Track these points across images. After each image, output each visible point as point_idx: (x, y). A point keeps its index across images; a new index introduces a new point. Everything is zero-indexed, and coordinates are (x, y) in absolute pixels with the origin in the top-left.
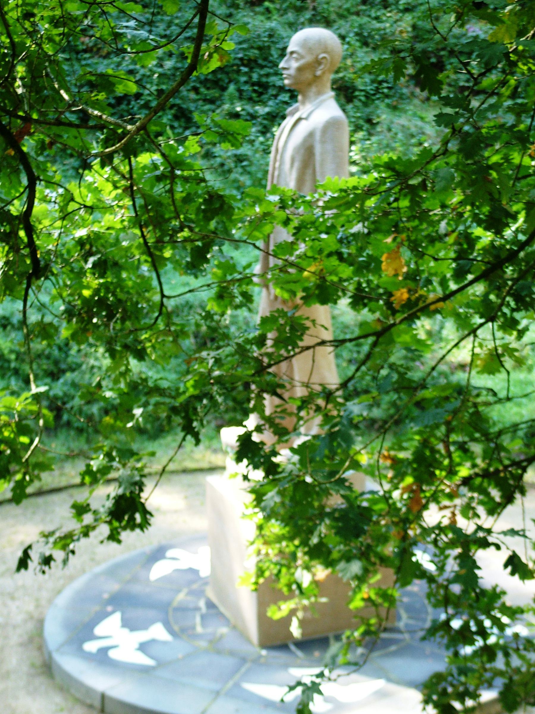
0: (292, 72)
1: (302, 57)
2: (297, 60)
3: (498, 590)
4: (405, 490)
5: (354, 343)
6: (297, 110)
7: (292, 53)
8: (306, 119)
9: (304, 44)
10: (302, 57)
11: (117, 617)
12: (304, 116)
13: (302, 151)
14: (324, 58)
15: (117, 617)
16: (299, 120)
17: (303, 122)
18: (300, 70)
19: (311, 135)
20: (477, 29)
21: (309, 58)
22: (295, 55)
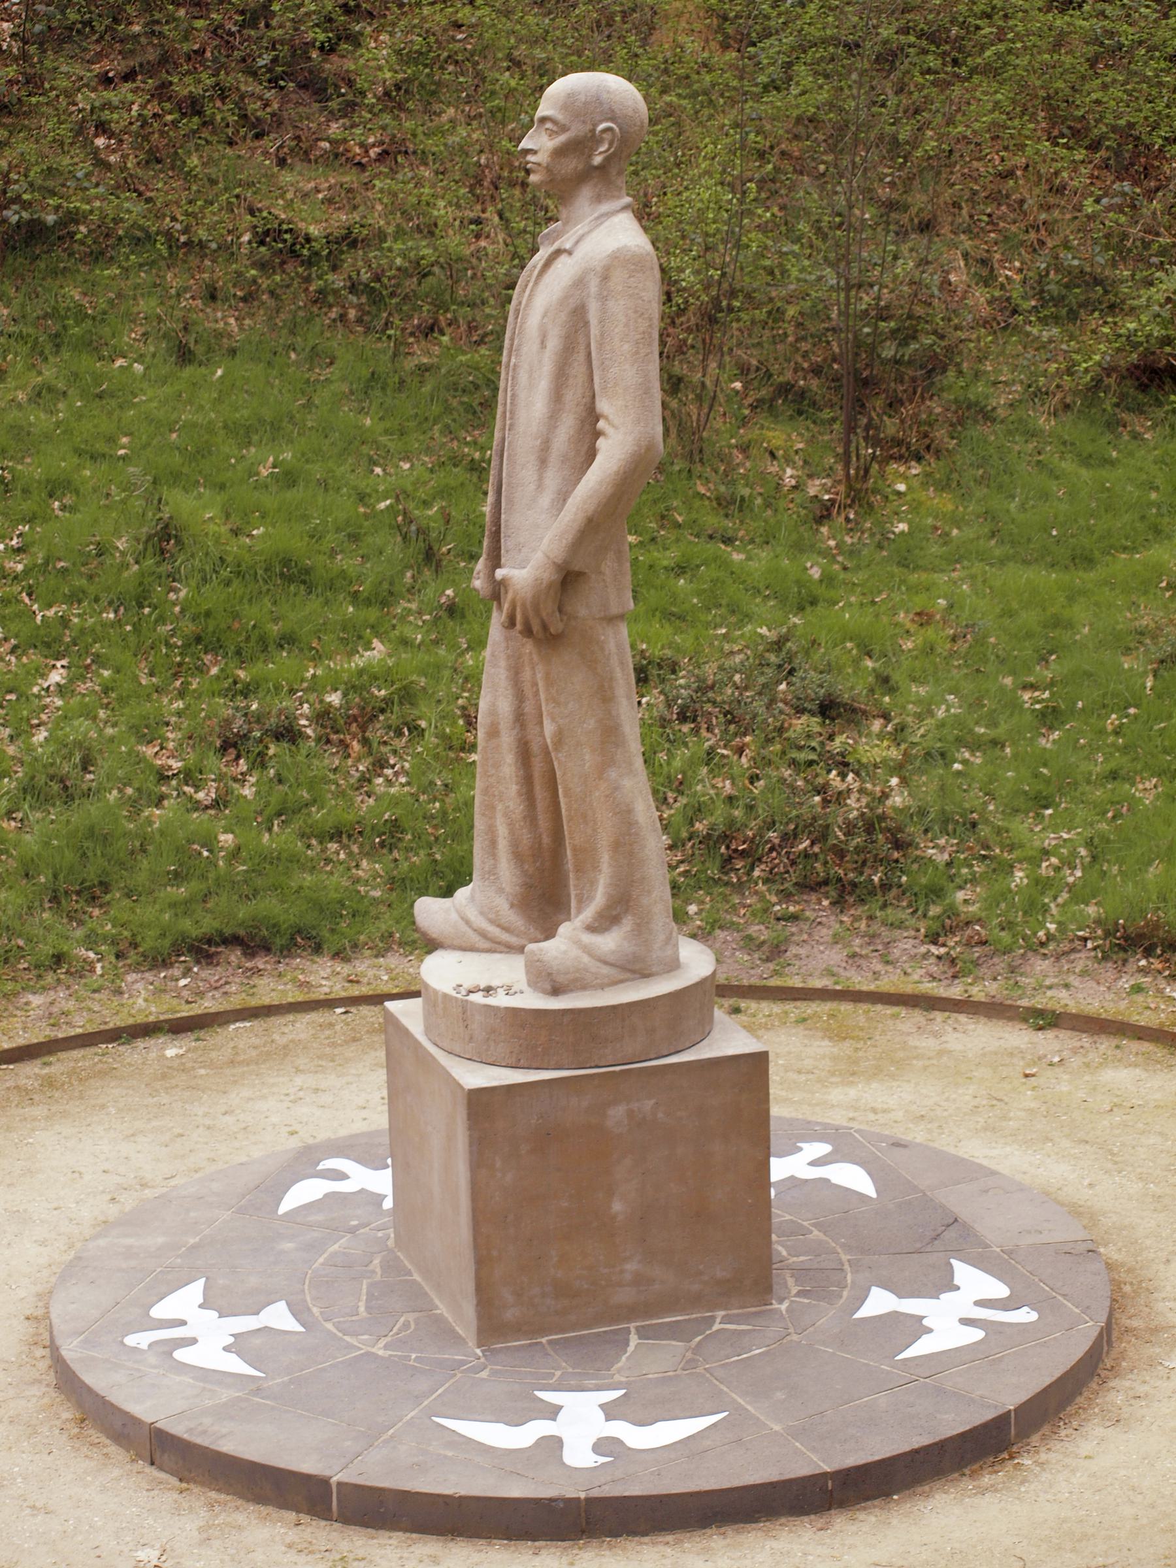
0: (541, 158)
1: (563, 129)
2: (552, 134)
3: (925, 1322)
4: (973, 755)
5: (314, 996)
6: (558, 235)
7: (543, 120)
8: (569, 253)
9: (569, 103)
10: (563, 129)
11: (195, 1290)
12: (568, 246)
13: (563, 316)
14: (609, 129)
15: (195, 1290)
16: (558, 252)
17: (563, 258)
18: (560, 153)
19: (580, 283)
20: (135, 107)
21: (577, 130)
22: (549, 125)
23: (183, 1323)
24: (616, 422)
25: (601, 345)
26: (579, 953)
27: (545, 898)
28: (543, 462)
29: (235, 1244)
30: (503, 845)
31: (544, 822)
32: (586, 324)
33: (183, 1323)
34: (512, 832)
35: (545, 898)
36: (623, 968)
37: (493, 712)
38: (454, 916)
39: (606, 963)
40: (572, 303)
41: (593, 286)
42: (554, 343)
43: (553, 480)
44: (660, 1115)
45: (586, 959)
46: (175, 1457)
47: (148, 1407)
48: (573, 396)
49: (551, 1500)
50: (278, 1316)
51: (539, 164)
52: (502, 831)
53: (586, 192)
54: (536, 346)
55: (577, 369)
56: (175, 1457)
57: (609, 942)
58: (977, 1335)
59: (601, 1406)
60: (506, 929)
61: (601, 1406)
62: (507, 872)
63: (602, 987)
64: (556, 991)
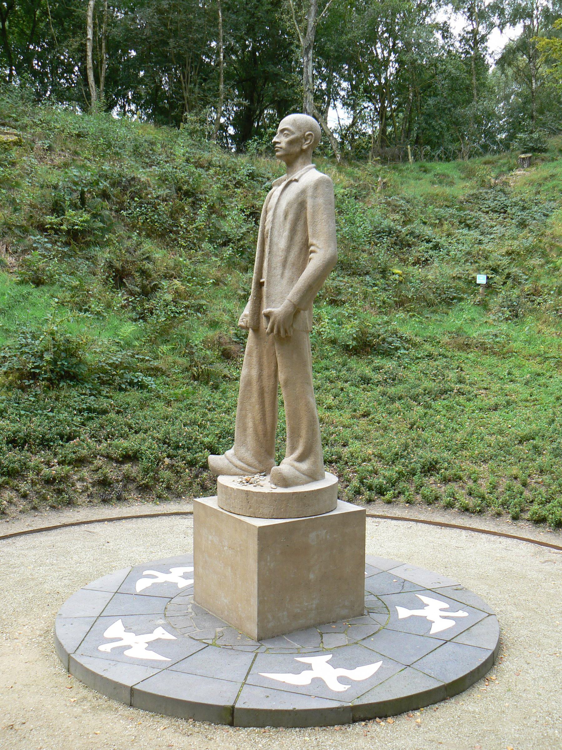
8: (296, 181)
10: (293, 133)
12: (296, 178)
21: (297, 134)
22: (285, 132)
23: (121, 639)
24: (320, 247)
25: (313, 217)
26: (294, 470)
27: (268, 451)
28: (284, 266)
29: (127, 604)
30: (250, 431)
31: (269, 420)
32: (306, 208)
33: (121, 639)
34: (254, 424)
35: (268, 451)
36: (310, 477)
37: (249, 375)
38: (226, 461)
39: (304, 474)
40: (300, 200)
41: (310, 193)
42: (290, 217)
43: (288, 274)
44: (328, 537)
45: (297, 473)
46: (136, 699)
47: (127, 677)
48: (298, 238)
49: (338, 708)
50: (160, 633)
51: (281, 148)
52: (250, 424)
53: (300, 160)
54: (282, 219)
55: (300, 228)
56: (136, 699)
57: (304, 466)
58: (451, 623)
59: (327, 662)
60: (249, 465)
61: (327, 662)
62: (250, 440)
63: (303, 484)
64: (286, 486)
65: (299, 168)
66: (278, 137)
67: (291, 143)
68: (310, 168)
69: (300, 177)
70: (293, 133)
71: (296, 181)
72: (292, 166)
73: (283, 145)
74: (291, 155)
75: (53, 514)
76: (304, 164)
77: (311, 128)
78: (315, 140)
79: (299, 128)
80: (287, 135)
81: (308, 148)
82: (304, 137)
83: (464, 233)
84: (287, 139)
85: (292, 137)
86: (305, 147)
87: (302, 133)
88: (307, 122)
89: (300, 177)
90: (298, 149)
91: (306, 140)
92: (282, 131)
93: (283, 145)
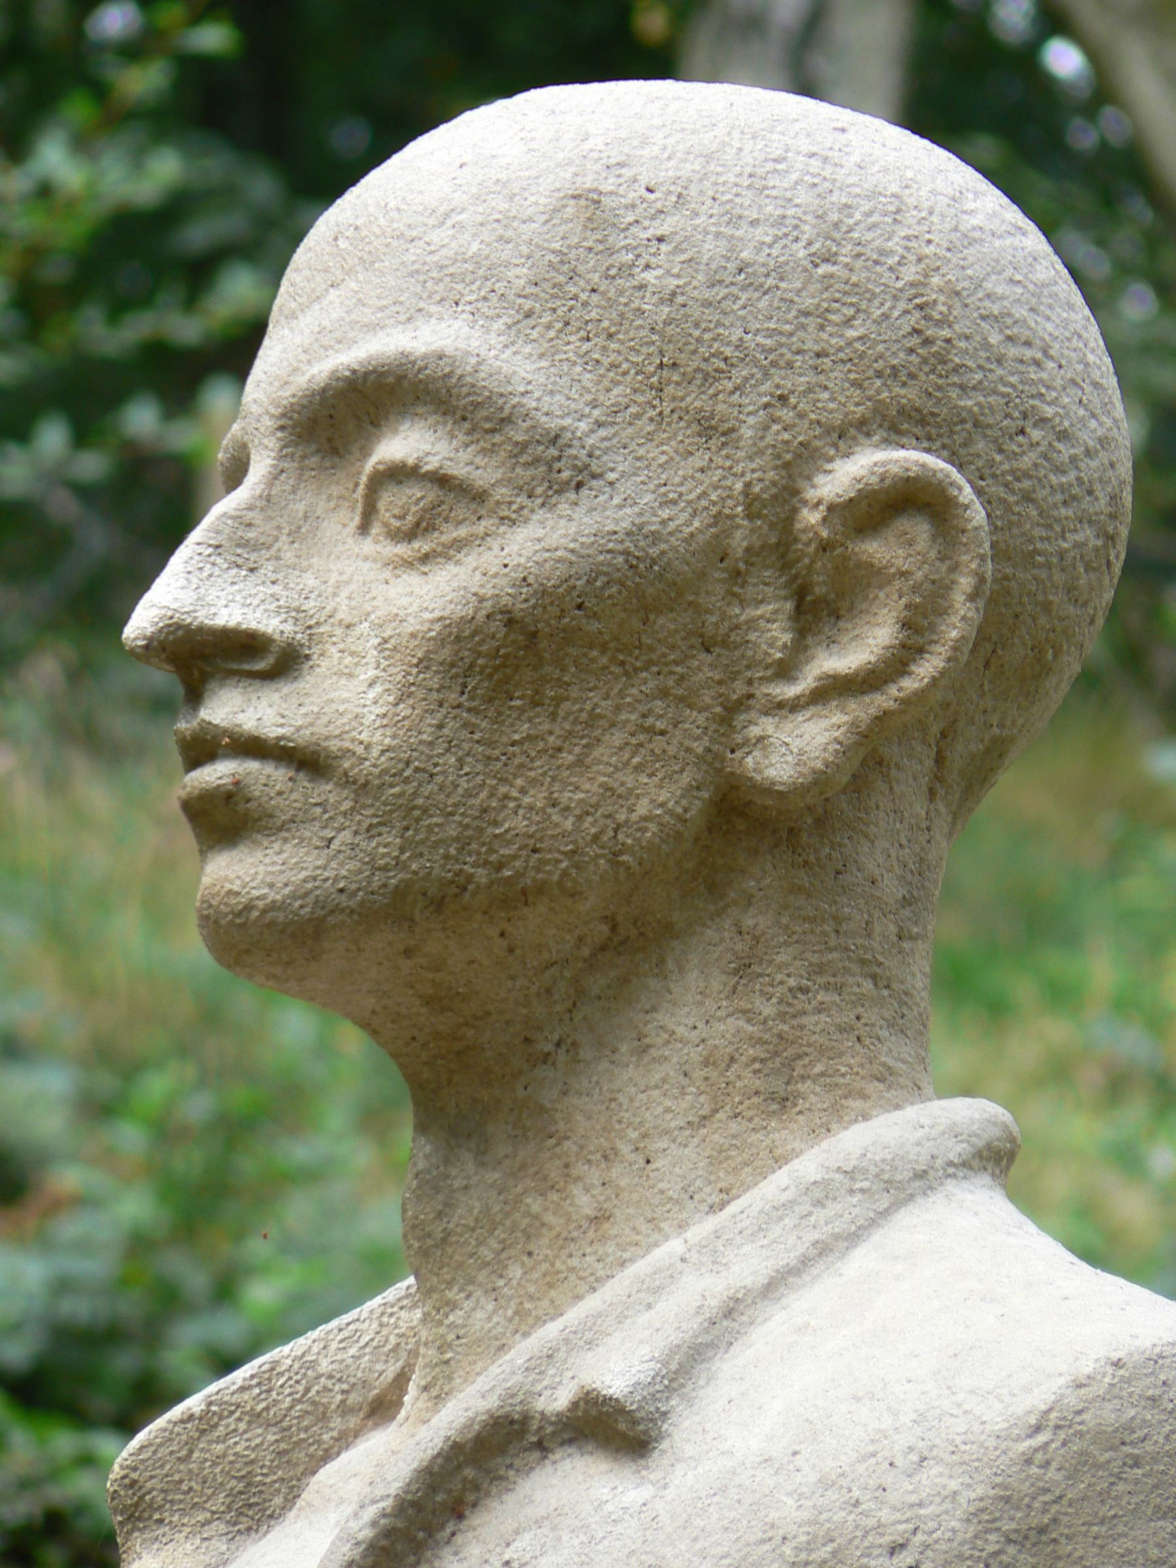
8: (615, 1430)
10: (554, 468)
12: (616, 1371)
22: (404, 443)
51: (307, 760)
53: (694, 1018)
65: (678, 1162)
66: (244, 551)
67: (505, 664)
68: (904, 1184)
69: (685, 1367)
70: (554, 468)
71: (615, 1430)
72: (534, 1123)
73: (350, 700)
74: (515, 897)
75: (887, 442)
76: (784, 1083)
77: (929, 379)
78: (1001, 607)
79: (679, 371)
80: (434, 512)
81: (866, 762)
82: (780, 547)
83: (613, 198)
84: (433, 594)
85: (531, 545)
86: (794, 747)
87: (752, 471)
88: (837, 253)
89: (685, 1367)
90: (658, 797)
91: (818, 612)
92: (340, 418)
93: (350, 700)
